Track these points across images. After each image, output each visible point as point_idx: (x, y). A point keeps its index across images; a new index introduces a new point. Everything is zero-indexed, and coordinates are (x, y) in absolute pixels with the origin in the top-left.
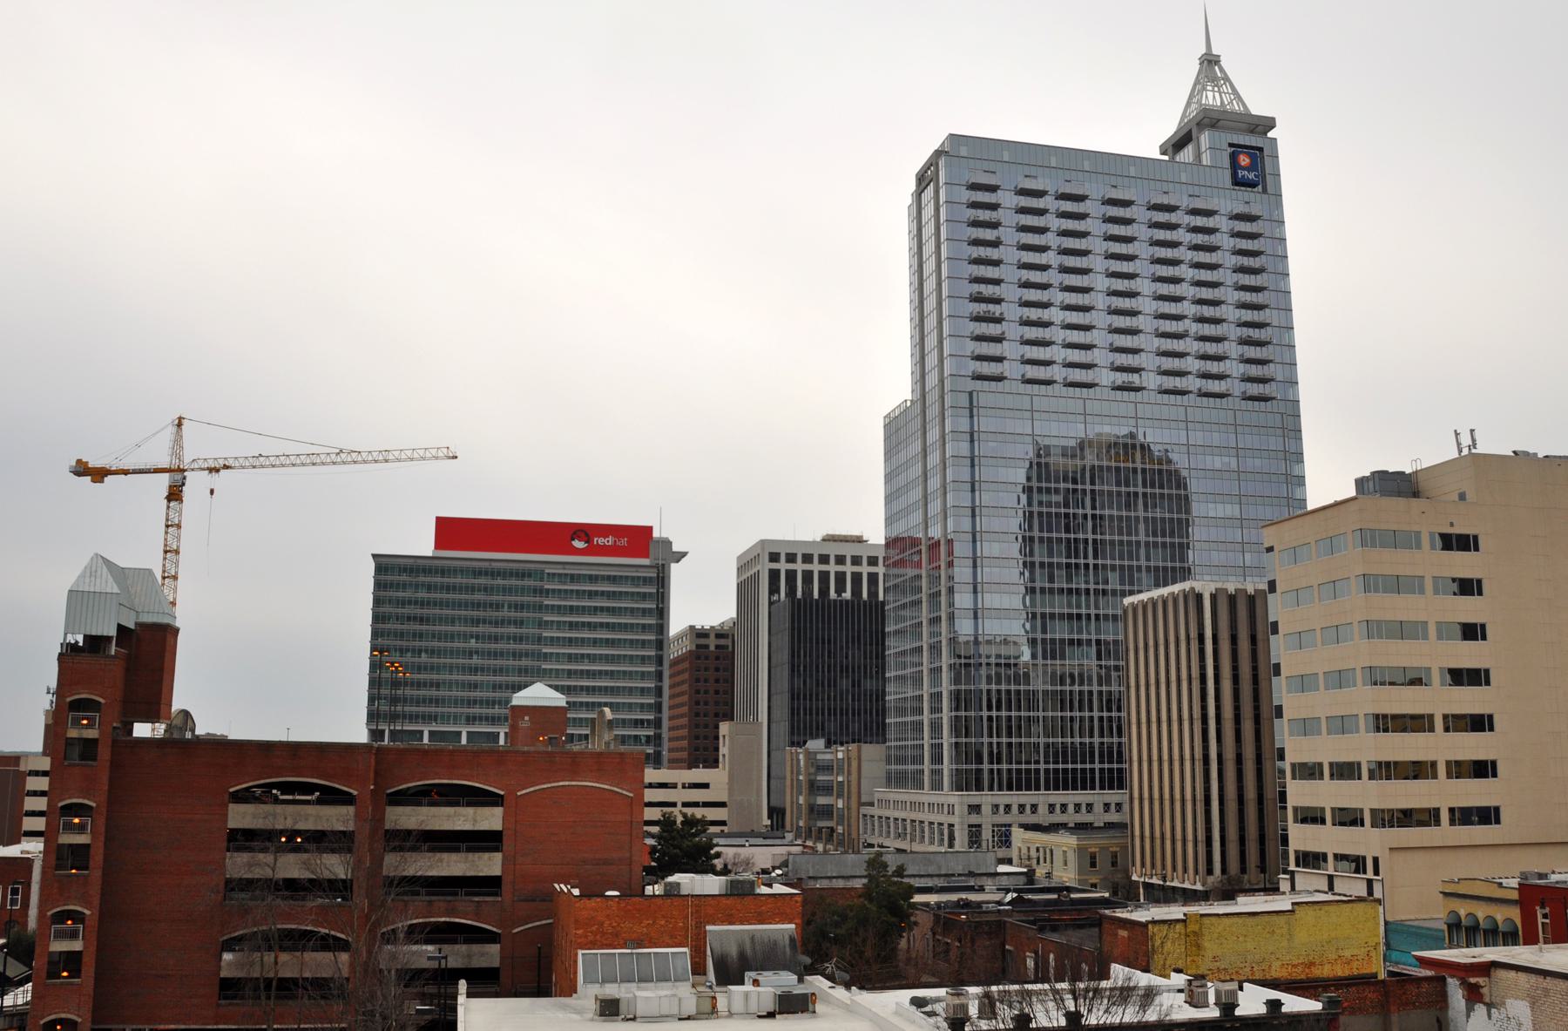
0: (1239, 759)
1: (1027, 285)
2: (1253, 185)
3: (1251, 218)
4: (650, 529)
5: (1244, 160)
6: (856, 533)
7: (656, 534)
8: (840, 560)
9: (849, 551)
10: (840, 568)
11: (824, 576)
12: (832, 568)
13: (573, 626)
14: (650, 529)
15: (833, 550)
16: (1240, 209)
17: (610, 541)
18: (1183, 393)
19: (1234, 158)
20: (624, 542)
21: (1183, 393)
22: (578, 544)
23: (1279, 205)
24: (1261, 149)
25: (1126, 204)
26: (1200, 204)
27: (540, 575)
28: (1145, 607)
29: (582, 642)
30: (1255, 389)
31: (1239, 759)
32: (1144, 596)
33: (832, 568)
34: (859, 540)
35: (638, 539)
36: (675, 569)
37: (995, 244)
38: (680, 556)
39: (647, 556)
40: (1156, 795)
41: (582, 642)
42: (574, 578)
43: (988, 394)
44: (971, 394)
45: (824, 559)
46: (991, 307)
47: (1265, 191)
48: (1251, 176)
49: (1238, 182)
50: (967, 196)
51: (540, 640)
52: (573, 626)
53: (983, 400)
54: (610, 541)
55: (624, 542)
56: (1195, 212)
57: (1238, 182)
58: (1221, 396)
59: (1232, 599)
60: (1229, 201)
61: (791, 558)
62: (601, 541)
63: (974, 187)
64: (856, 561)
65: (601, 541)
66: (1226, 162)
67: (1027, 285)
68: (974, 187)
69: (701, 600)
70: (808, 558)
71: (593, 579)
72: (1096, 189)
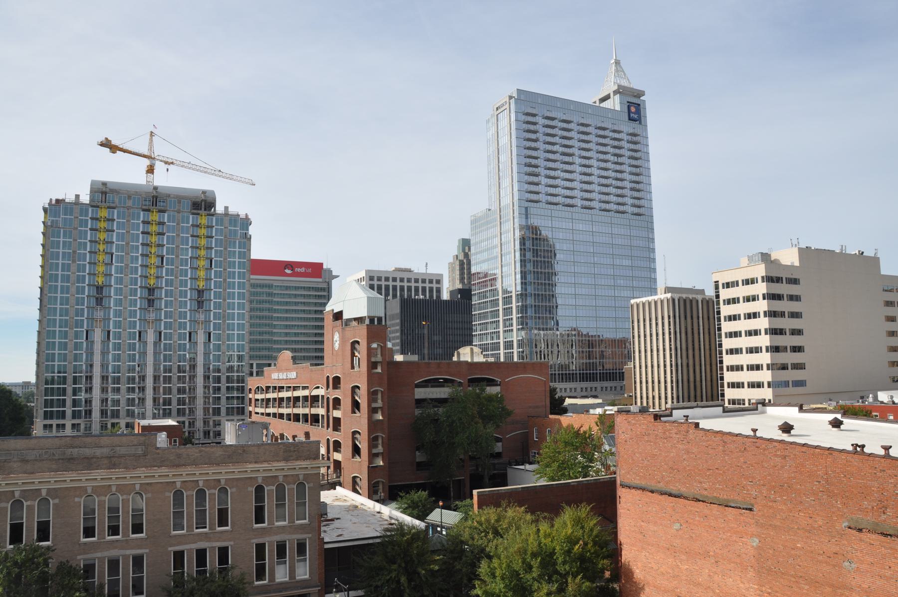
0: (688, 365)
1: (548, 160)
2: (635, 120)
3: (635, 135)
4: (321, 264)
5: (633, 109)
6: (408, 267)
7: (325, 267)
8: (402, 280)
9: (406, 276)
10: (395, 284)
11: (409, 288)
12: (398, 284)
13: (287, 311)
14: (321, 264)
15: (398, 275)
16: (631, 131)
17: (303, 270)
18: (608, 211)
19: (629, 107)
20: (309, 270)
21: (608, 211)
22: (288, 271)
23: (646, 130)
24: (639, 105)
25: (587, 125)
26: (616, 128)
27: (270, 286)
28: (644, 304)
29: (293, 319)
30: (587, 203)
31: (688, 365)
32: (644, 299)
33: (398, 284)
34: (410, 271)
35: (316, 269)
36: (334, 282)
37: (536, 140)
38: (337, 277)
39: (320, 277)
40: (692, 379)
41: (293, 319)
42: (287, 288)
43: (534, 209)
44: (526, 208)
45: (394, 280)
46: (534, 169)
47: (640, 123)
48: (636, 116)
49: (630, 119)
50: (524, 118)
51: (271, 318)
52: (287, 311)
53: (532, 211)
54: (303, 270)
55: (309, 270)
56: (614, 131)
57: (630, 119)
58: (536, 202)
59: (685, 301)
60: (628, 127)
61: (424, 281)
62: (299, 270)
63: (528, 114)
64: (409, 280)
65: (299, 270)
66: (626, 110)
67: (548, 160)
68: (528, 114)
69: (351, 299)
70: (387, 279)
71: (297, 288)
72: (541, 111)
